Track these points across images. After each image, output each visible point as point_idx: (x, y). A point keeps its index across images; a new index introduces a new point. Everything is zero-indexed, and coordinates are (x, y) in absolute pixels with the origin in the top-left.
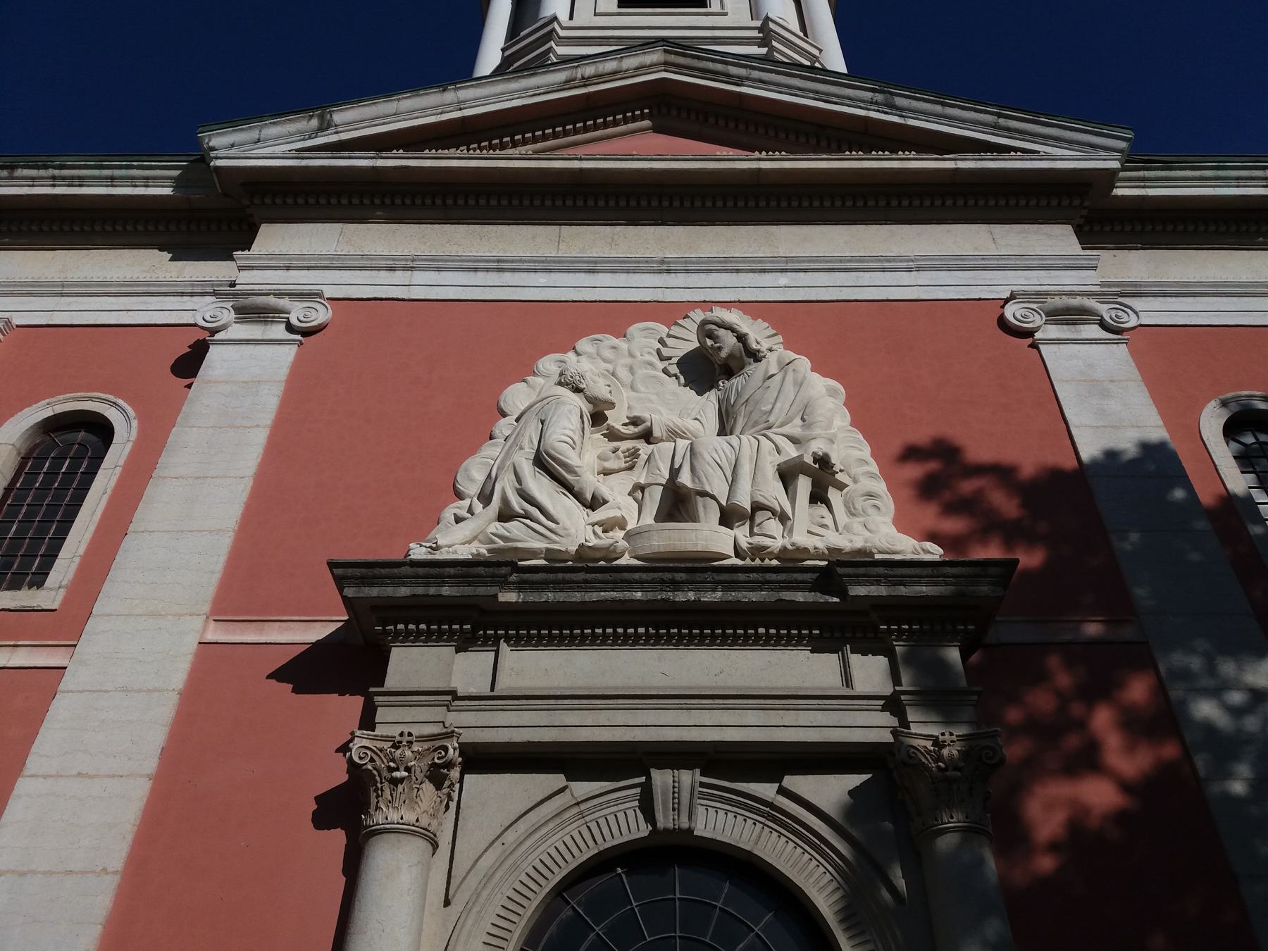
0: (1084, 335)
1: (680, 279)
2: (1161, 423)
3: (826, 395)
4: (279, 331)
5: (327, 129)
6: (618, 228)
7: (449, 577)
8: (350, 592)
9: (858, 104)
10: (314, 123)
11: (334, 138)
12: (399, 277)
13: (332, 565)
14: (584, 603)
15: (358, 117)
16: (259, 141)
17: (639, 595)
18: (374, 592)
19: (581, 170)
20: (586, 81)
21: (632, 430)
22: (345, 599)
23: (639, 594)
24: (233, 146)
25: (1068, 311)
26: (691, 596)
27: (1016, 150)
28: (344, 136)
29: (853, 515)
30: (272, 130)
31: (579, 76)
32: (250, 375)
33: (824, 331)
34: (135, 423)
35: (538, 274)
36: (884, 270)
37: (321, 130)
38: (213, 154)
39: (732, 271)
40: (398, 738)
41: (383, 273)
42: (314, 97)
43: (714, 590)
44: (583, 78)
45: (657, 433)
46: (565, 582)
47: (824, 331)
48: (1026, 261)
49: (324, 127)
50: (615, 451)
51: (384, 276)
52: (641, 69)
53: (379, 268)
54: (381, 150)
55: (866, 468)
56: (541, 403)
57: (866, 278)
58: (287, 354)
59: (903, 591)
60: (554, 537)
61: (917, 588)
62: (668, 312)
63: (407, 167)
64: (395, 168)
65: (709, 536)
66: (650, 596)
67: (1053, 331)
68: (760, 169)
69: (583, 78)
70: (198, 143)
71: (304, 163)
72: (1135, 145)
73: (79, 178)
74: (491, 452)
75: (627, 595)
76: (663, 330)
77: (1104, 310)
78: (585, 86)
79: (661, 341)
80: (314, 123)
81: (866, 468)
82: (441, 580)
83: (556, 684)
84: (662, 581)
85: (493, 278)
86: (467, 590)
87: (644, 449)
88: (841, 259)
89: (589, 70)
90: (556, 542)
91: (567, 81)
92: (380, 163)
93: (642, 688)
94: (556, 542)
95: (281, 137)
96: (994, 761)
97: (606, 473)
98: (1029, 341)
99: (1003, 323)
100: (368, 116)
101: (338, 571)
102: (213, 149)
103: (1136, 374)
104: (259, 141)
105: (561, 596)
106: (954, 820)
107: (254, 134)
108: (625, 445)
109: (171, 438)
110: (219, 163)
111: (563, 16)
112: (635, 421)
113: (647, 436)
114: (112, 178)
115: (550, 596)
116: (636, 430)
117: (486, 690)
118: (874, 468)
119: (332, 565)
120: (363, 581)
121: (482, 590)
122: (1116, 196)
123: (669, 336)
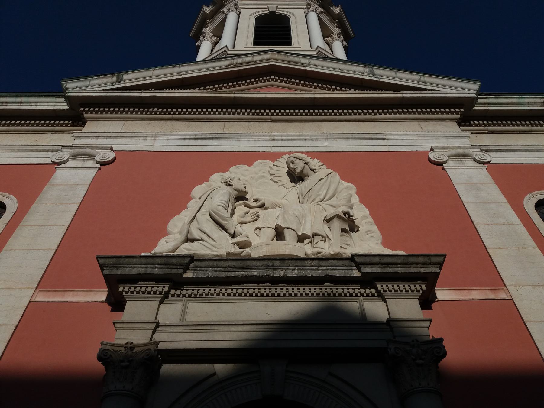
0: (466, 165)
1: (279, 143)
2: (506, 201)
3: (347, 190)
4: (90, 163)
5: (120, 82)
6: (251, 123)
7: (158, 264)
8: (106, 272)
9: (357, 71)
10: (115, 79)
11: (124, 85)
12: (149, 142)
13: (98, 258)
14: (227, 277)
15: (134, 77)
16: (89, 86)
17: (255, 273)
18: (119, 272)
19: (234, 98)
20: (237, 65)
21: (255, 204)
22: (105, 276)
23: (256, 273)
24: (77, 87)
25: (458, 155)
26: (282, 273)
27: (429, 90)
28: (128, 85)
29: (362, 240)
30: (95, 81)
31: (235, 63)
32: (74, 181)
33: (344, 164)
34: (11, 196)
35: (214, 141)
36: (372, 139)
37: (117, 82)
38: (67, 91)
39: (302, 139)
40: (126, 345)
41: (141, 140)
42: (116, 68)
43: (294, 270)
44: (237, 64)
45: (266, 205)
46: (218, 267)
47: (344, 164)
48: (438, 137)
49: (119, 80)
50: (247, 213)
51: (142, 142)
52: (262, 61)
53: (140, 138)
54: (144, 89)
55: (368, 220)
56: (212, 193)
57: (364, 142)
58: (92, 173)
59: (389, 270)
60: (214, 249)
61: (396, 269)
62: (273, 156)
63: (155, 96)
64: (150, 96)
65: (289, 247)
66: (261, 274)
67: (451, 163)
68: (315, 98)
69: (237, 64)
70: (61, 86)
71: (108, 94)
72: (481, 87)
73: (6, 102)
74: (186, 215)
75: (250, 273)
76: (272, 164)
77: (475, 154)
78: (237, 67)
79: (270, 167)
80: (115, 79)
81: (368, 220)
82: (154, 265)
83: (211, 320)
84: (267, 266)
85: (192, 142)
86: (167, 271)
87: (261, 212)
88: (352, 134)
89: (239, 61)
90: (215, 251)
91: (229, 65)
92: (143, 94)
93: (256, 321)
94: (215, 251)
95: (98, 85)
96: (441, 354)
97: (242, 223)
98: (441, 167)
99: (430, 160)
100: (139, 77)
101: (102, 261)
102: (67, 89)
103: (492, 181)
104: (89, 86)
105: (216, 274)
106: (424, 288)
107: (87, 83)
108: (252, 211)
109: (32, 208)
110: (69, 94)
111: (230, 47)
112: (256, 200)
113: (262, 206)
114: (21, 102)
115: (210, 274)
116: (258, 204)
117: (176, 321)
118: (371, 219)
119: (98, 258)
120: (114, 266)
121: (174, 271)
122: (475, 110)
123: (274, 165)
